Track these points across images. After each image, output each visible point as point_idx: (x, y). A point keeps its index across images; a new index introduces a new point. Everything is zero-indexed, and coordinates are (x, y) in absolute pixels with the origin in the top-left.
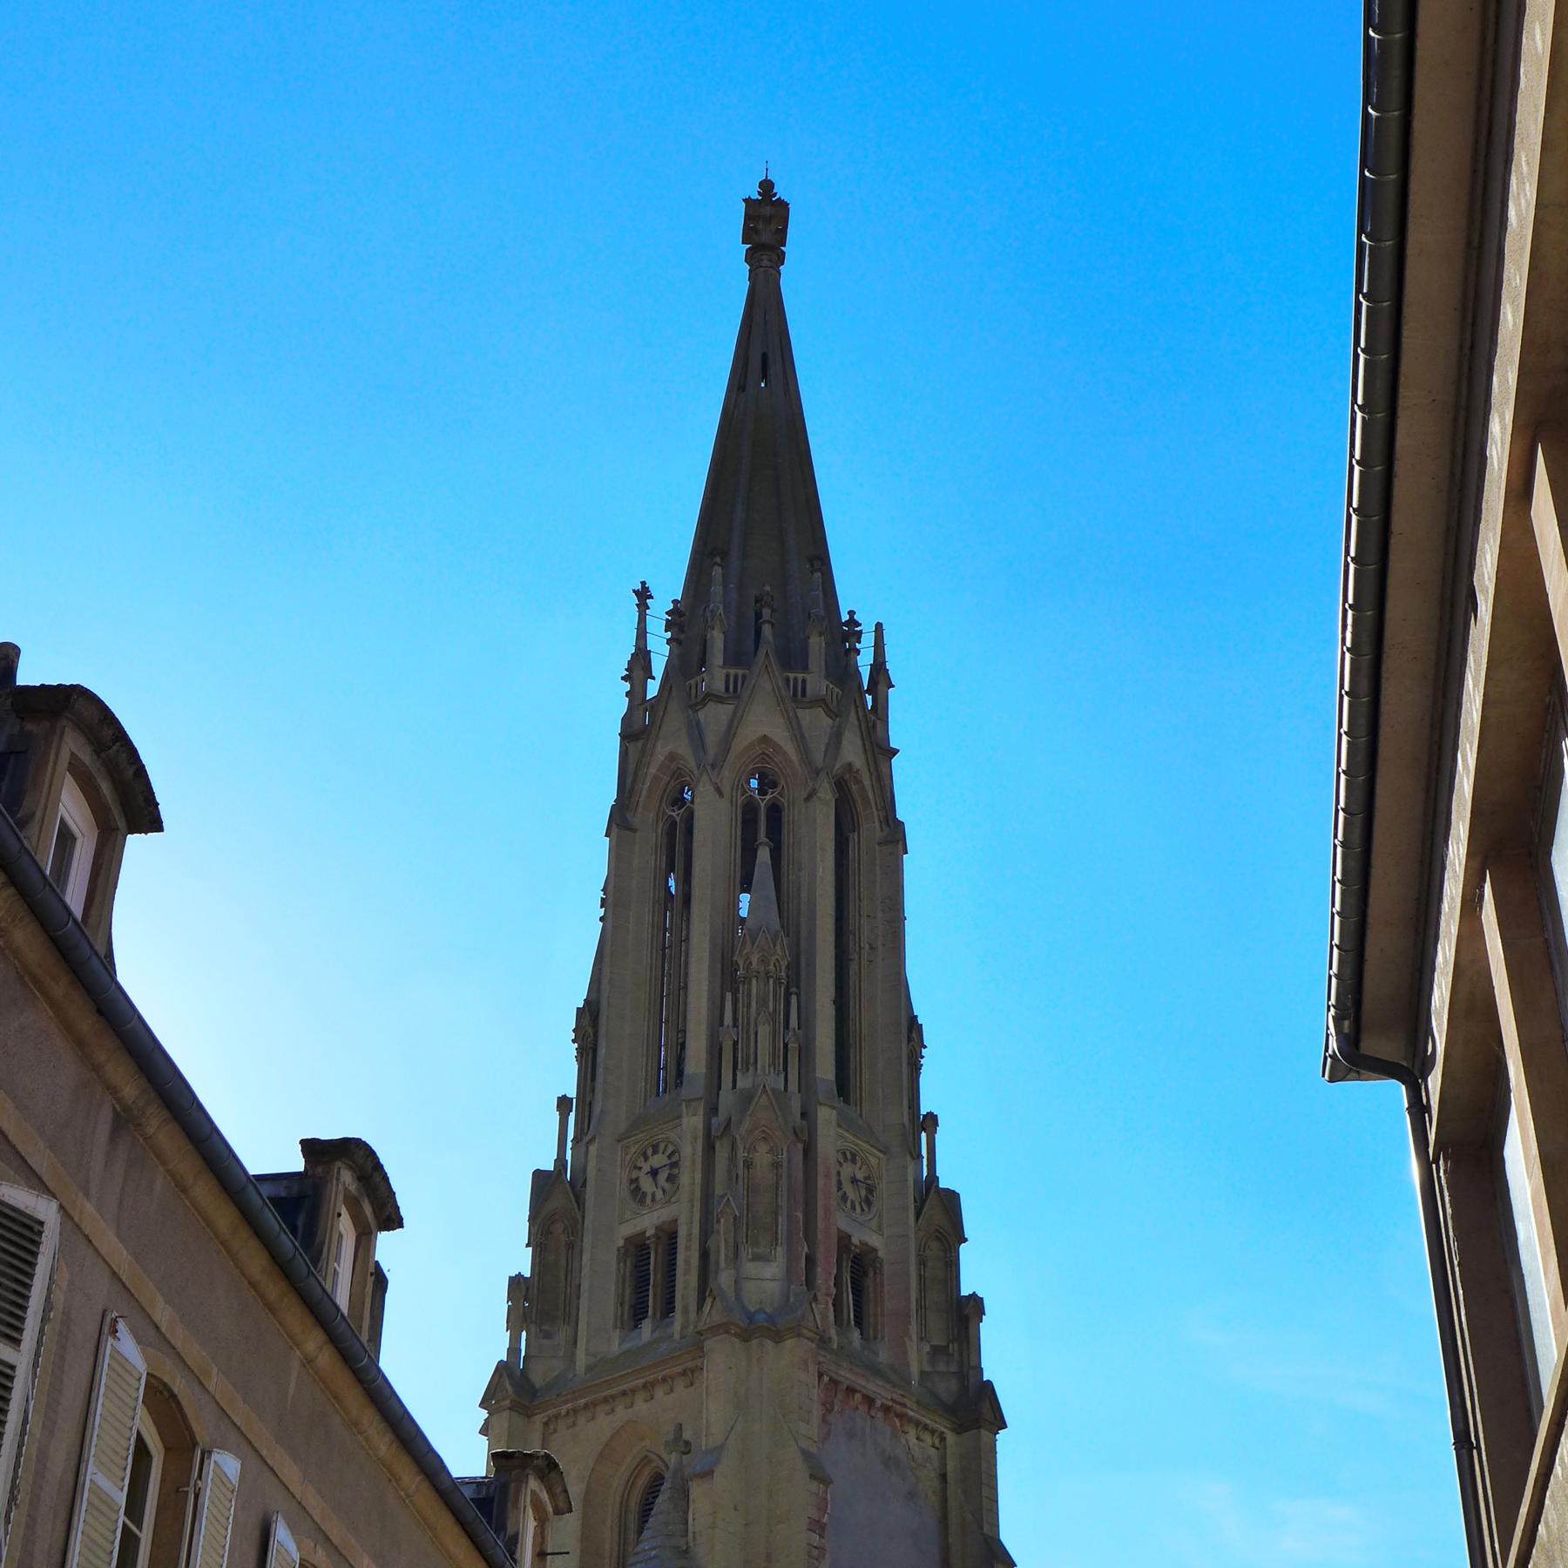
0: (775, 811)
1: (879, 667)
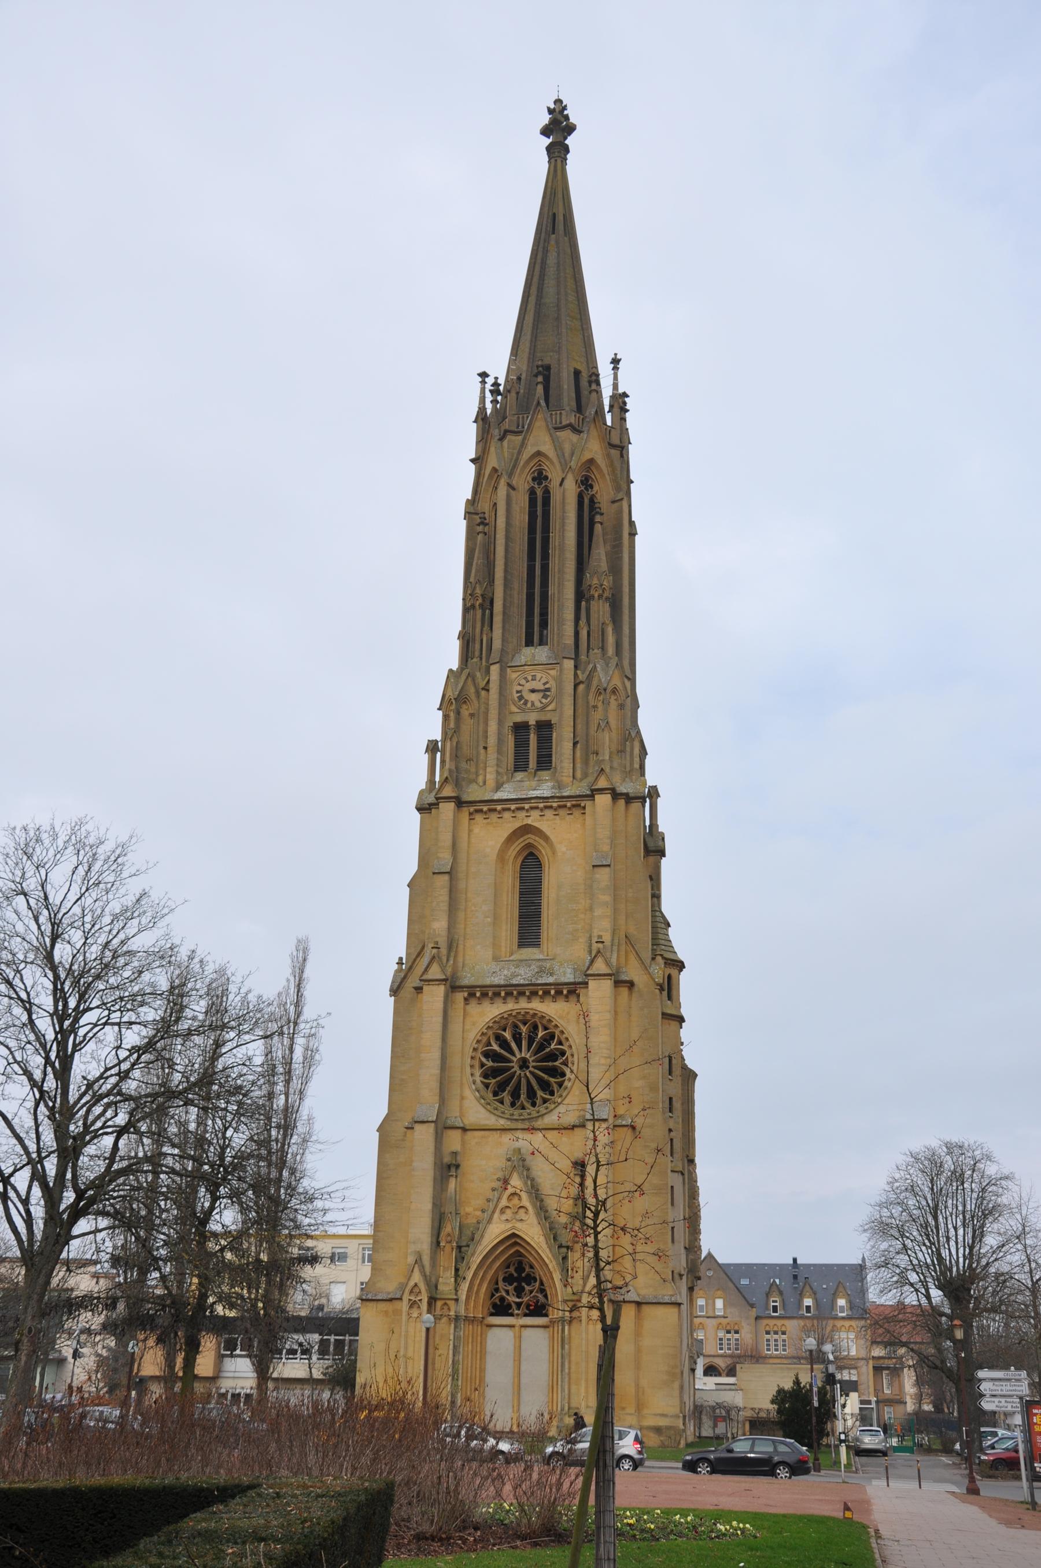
0: (547, 492)
1: (620, 402)
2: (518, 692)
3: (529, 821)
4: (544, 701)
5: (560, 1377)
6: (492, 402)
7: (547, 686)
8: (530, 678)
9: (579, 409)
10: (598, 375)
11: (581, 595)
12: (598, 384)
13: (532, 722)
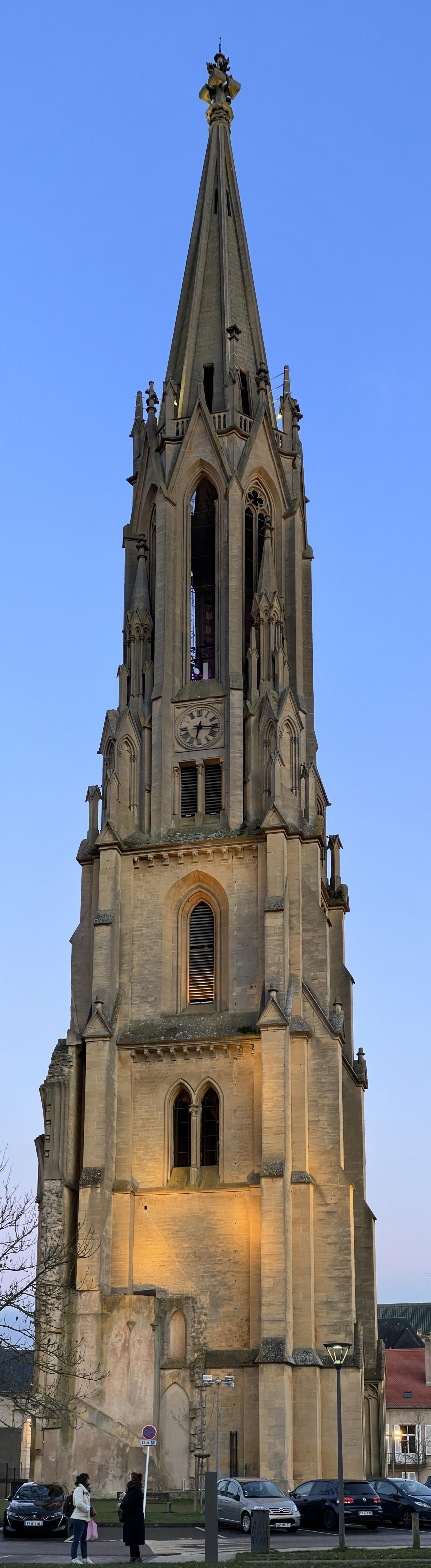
2: (182, 730)
4: (211, 738)
5: (297, 758)
6: (148, 410)
7: (214, 722)
8: (195, 714)
9: (246, 409)
10: (266, 372)
11: (250, 622)
12: (267, 383)
13: (199, 762)
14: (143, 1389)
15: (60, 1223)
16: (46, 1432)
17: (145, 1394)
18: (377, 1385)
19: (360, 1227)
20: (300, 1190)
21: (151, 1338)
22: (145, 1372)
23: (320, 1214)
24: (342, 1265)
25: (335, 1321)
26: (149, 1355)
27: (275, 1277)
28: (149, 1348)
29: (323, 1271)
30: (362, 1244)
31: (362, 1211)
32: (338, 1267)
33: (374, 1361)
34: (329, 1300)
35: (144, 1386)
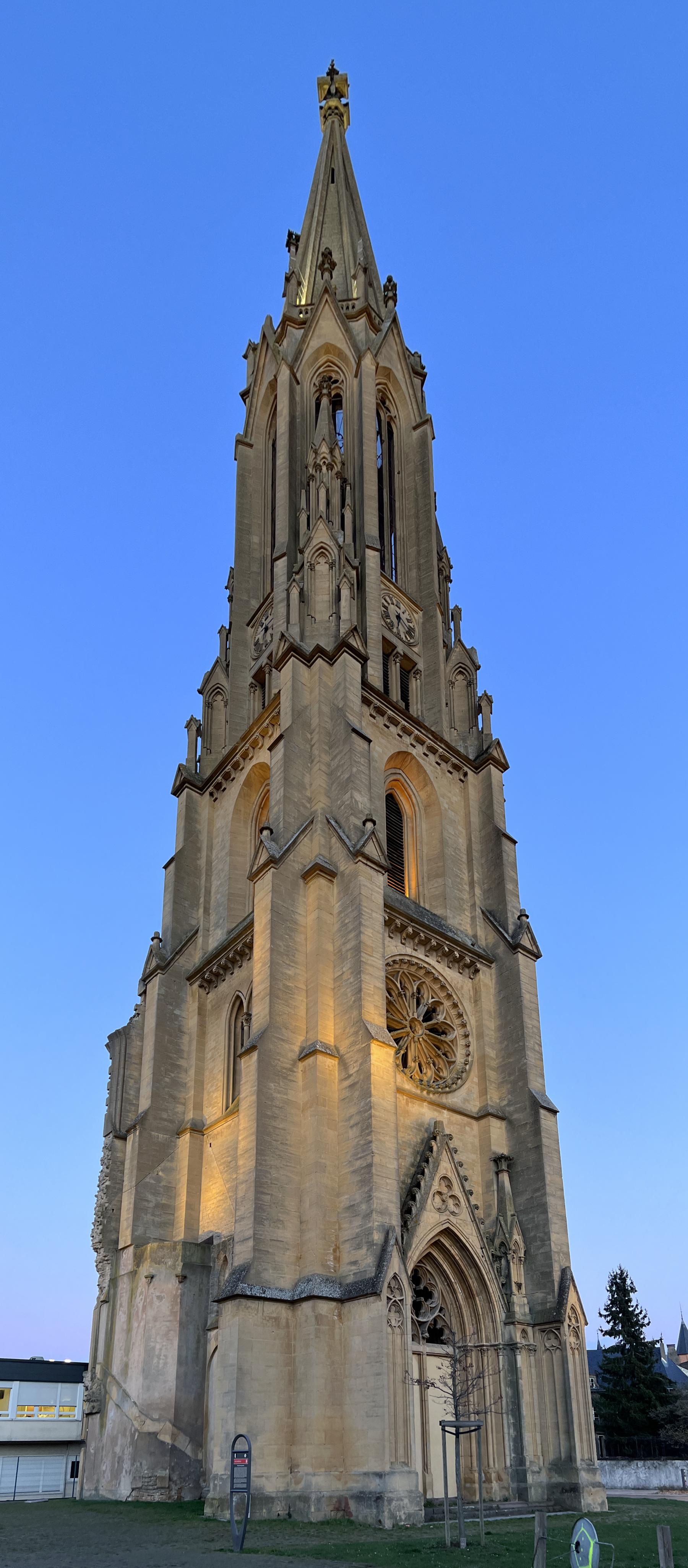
3: (414, 752)
14: (162, 1357)
15: (108, 1178)
16: (90, 1418)
17: (165, 1364)
18: (558, 1329)
19: (526, 1123)
20: (309, 1065)
21: (177, 1292)
22: (166, 1334)
23: (344, 1092)
24: (363, 1151)
25: (357, 1231)
26: (173, 1313)
27: (247, 1181)
28: (172, 1305)
29: (346, 1165)
30: (529, 1145)
31: (527, 1103)
32: (359, 1156)
33: (554, 1297)
34: (352, 1204)
35: (163, 1353)
